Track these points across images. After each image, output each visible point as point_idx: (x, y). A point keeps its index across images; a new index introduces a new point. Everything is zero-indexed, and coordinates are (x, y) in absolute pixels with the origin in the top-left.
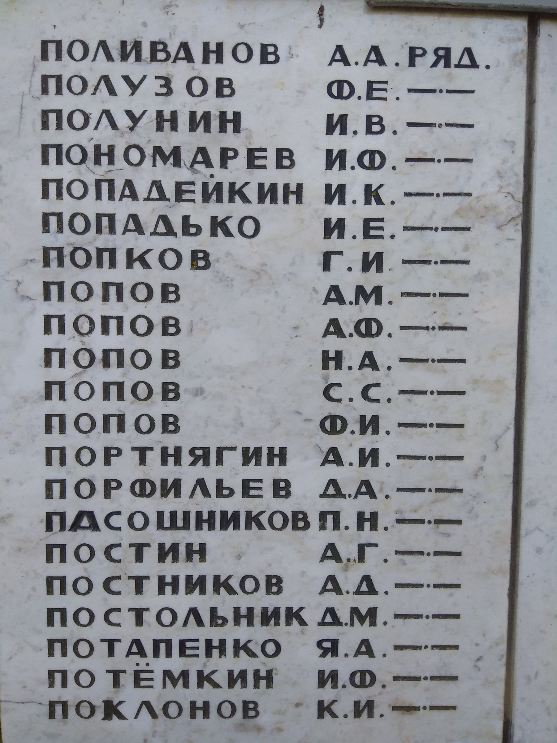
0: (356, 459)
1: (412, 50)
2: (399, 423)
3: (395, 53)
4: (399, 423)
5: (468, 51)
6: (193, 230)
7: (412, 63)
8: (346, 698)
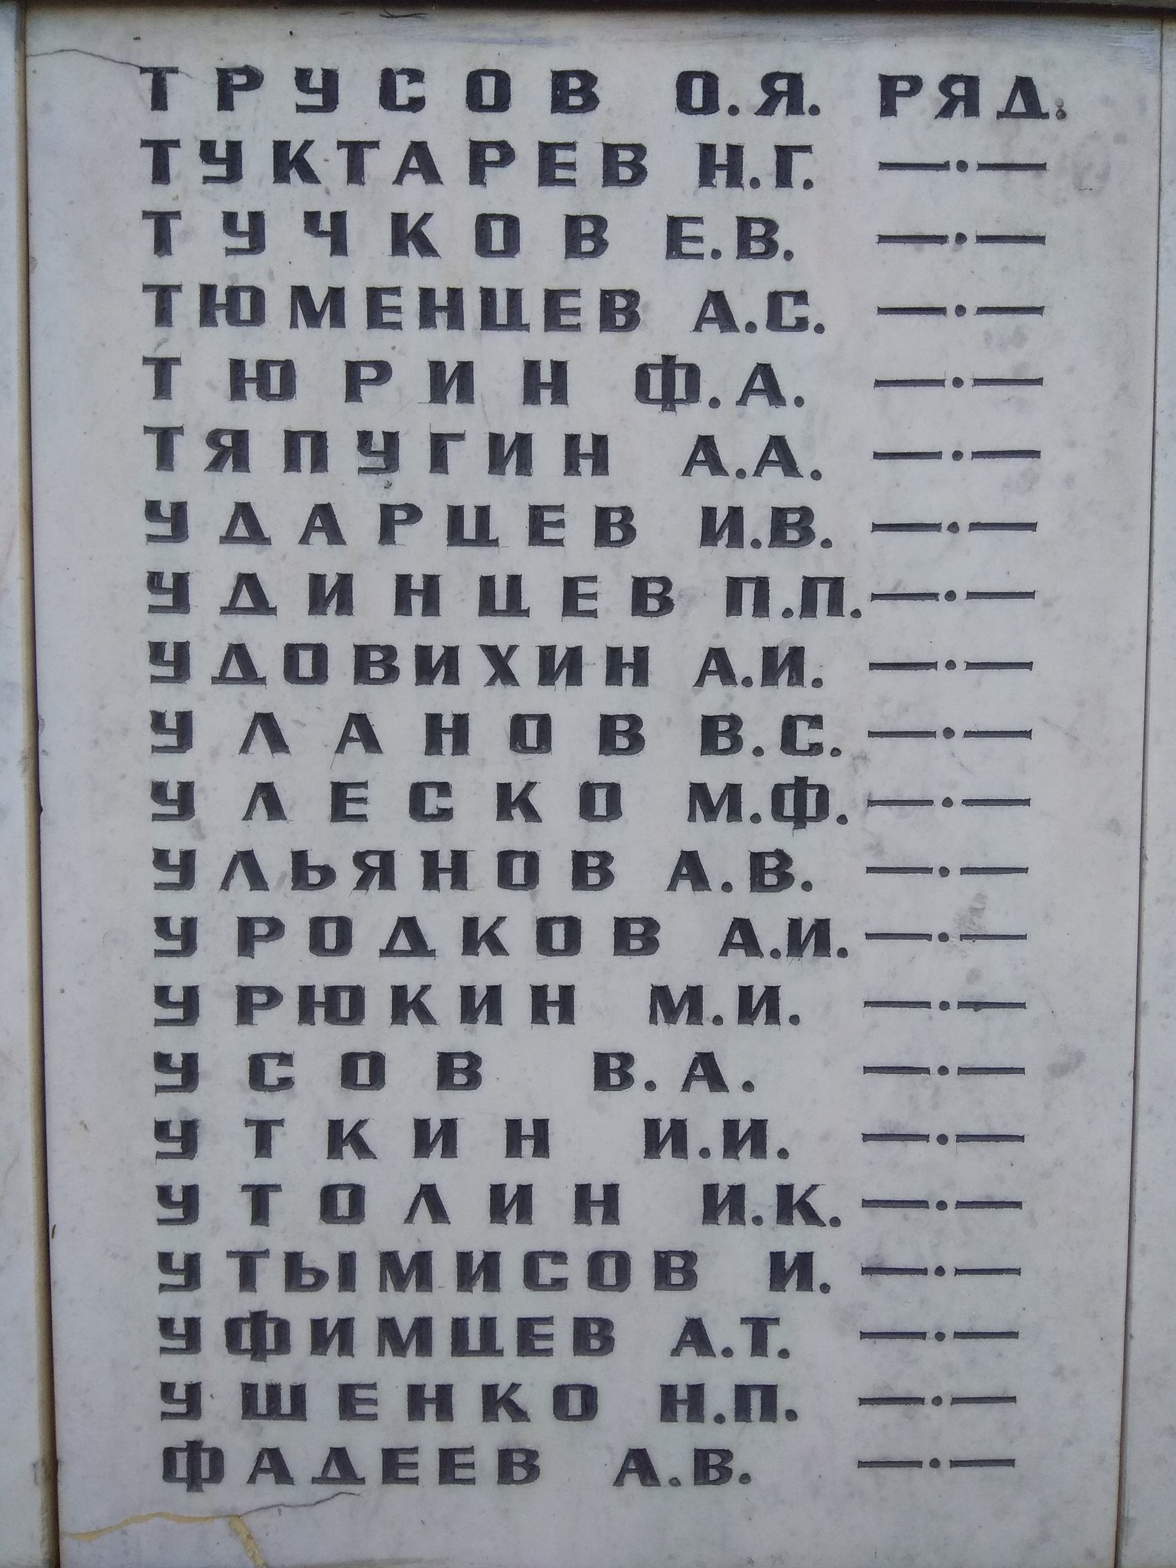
0: (781, 940)
5: (1024, 86)
6: (314, 877)
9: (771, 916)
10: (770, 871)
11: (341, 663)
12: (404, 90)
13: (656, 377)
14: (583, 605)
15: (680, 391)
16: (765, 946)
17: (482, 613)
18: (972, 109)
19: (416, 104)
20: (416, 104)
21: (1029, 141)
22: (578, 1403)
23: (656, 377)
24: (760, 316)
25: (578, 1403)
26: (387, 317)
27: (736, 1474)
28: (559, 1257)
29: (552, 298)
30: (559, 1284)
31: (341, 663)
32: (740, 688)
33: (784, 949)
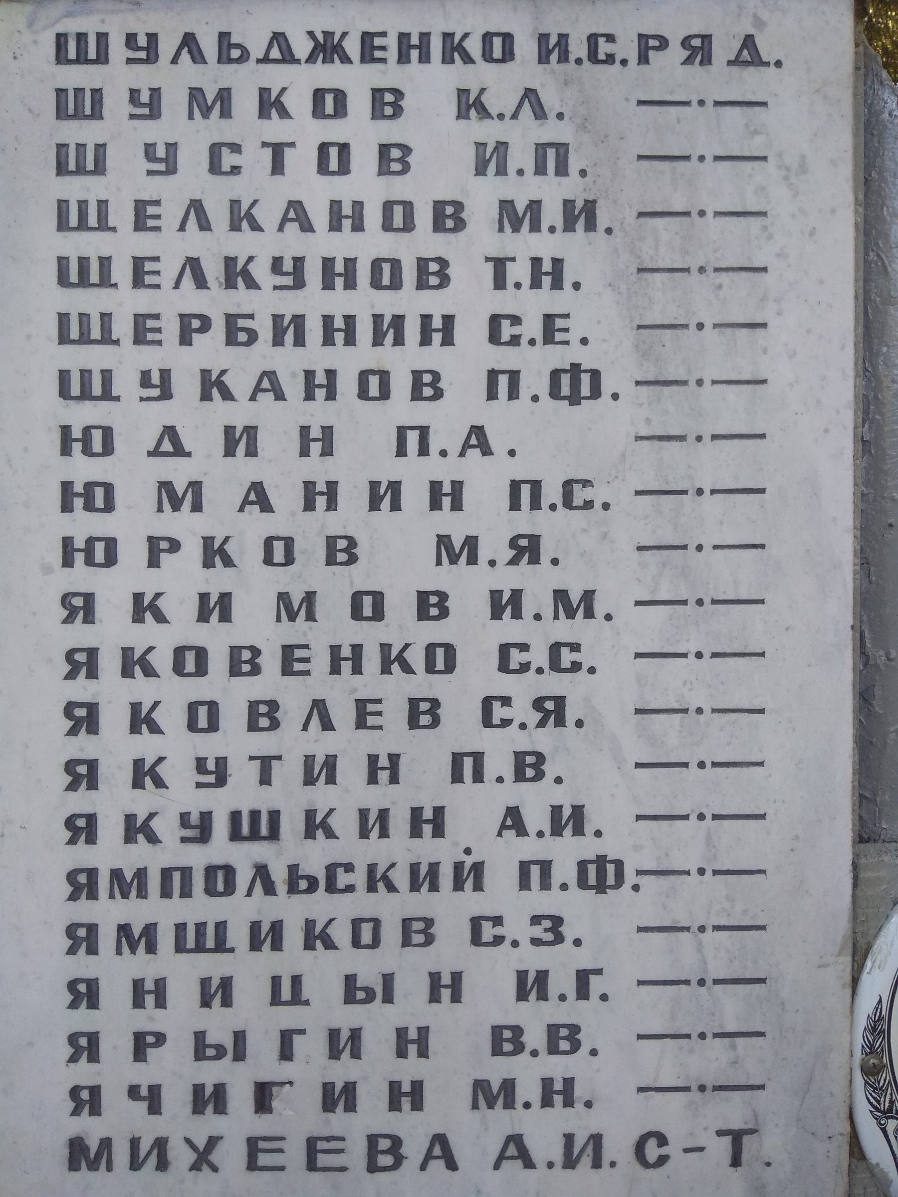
1: (643, 38)
2: (638, 981)
3: (627, 48)
4: (638, 981)
7: (643, 59)
8: (544, 1131)
9: (535, 802)
10: (529, 766)
11: (401, 385)
12: (228, 159)
13: (565, 380)
14: (558, 336)
15: (585, 390)
16: (532, 829)
17: (518, 372)
18: (707, 60)
19: (235, 170)
20: (235, 170)
21: (750, 83)
22: (423, 713)
23: (565, 380)
24: (583, 53)
25: (423, 713)
26: (150, 223)
27: (528, 1049)
28: (349, 868)
29: (140, 206)
30: (350, 889)
31: (401, 385)
32: (496, 122)
33: (547, 830)
